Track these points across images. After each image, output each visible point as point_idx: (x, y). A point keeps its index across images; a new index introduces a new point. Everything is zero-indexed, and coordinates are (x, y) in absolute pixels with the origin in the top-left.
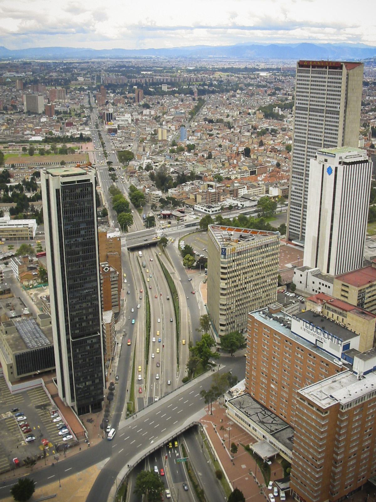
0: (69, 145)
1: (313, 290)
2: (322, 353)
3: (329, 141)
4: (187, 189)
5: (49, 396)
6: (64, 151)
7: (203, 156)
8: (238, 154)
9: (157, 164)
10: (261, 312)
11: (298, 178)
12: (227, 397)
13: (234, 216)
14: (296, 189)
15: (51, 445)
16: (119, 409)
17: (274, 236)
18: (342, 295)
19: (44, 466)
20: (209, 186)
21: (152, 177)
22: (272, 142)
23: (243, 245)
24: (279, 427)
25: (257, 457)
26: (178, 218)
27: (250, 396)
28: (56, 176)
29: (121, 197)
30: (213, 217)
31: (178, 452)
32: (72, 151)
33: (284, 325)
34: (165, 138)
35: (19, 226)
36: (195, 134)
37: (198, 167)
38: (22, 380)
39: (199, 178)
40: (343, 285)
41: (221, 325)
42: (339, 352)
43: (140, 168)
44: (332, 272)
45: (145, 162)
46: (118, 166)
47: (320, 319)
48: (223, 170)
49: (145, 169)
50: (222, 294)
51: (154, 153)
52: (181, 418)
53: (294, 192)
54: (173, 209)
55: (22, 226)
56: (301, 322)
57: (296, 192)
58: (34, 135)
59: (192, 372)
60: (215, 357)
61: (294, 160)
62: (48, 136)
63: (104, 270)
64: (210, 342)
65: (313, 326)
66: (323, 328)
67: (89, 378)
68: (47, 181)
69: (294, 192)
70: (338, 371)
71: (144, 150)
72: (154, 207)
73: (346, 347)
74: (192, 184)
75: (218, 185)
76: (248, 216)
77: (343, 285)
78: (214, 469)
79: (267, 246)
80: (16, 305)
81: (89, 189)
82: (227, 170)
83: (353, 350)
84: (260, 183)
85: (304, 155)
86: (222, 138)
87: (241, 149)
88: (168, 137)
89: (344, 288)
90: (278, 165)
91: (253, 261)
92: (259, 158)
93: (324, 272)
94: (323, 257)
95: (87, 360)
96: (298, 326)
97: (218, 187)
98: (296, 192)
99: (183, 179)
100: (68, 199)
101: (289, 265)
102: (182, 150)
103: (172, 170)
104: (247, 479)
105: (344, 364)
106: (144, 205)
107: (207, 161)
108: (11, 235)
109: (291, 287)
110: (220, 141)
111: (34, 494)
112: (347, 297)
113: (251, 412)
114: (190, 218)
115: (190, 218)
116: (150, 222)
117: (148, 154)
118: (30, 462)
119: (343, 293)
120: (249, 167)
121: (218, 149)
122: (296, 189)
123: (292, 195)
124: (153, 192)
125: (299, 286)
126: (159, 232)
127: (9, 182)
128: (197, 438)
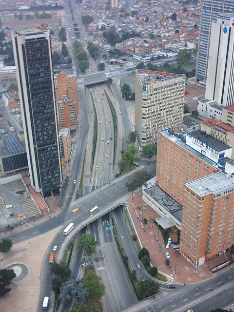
0: (48, 12)
1: (211, 116)
2: (205, 160)
3: (228, 8)
4: (129, 43)
5: (25, 185)
6: (44, 17)
7: (143, 19)
8: (167, 18)
9: (109, 25)
10: (167, 131)
11: (205, 36)
12: (144, 188)
13: (160, 63)
14: (203, 44)
15: (25, 217)
16: (72, 194)
17: (181, 78)
18: (228, 120)
19: (20, 231)
20: (145, 41)
21: (105, 35)
22: (193, 9)
23: (159, 84)
24: (177, 208)
25: (160, 228)
26: (121, 65)
27: (159, 187)
28: (21, 35)
29: (82, 49)
30: (145, 64)
31: (109, 222)
32: (49, 16)
33: (182, 140)
34: (116, 6)
35: (10, 71)
36: (138, 3)
37: (138, 27)
38: (8, 175)
39: (138, 35)
40: (229, 113)
41: (143, 139)
42: (216, 158)
43: (97, 28)
44: (225, 104)
45: (100, 24)
46: (81, 27)
47: (205, 136)
48: (156, 29)
49: (100, 29)
50: (143, 118)
51: (108, 18)
52: (111, 200)
53: (201, 46)
54: (117, 58)
55: (12, 71)
56: (193, 138)
57: (203, 46)
58: (23, 5)
59: (122, 171)
60: (138, 160)
61: (202, 22)
62: (33, 5)
63: (64, 100)
64: (134, 151)
65: (200, 141)
66: (207, 142)
67: (50, 173)
68: (16, 38)
69: (201, 46)
70: (215, 172)
71: (101, 15)
72: (105, 56)
73: (222, 156)
74: (133, 40)
75: (151, 41)
76: (170, 63)
77: (229, 113)
78: (132, 234)
79: (175, 84)
80: (5, 125)
81: (45, 44)
82: (159, 30)
83: (227, 158)
84: (181, 39)
85: (209, 18)
86: (157, 6)
87: (170, 14)
88: (118, 5)
89: (229, 119)
90: (196, 26)
91: (165, 95)
92: (183, 21)
93: (219, 103)
94: (218, 92)
95: (49, 161)
96: (190, 141)
97: (151, 42)
98: (203, 46)
99: (126, 36)
100: (30, 52)
101: (196, 99)
102: (128, 15)
103: (119, 29)
104: (152, 241)
105: (219, 167)
106: (97, 55)
107: (145, 23)
108: (4, 77)
109: (195, 114)
110: (156, 9)
111: (12, 248)
112: (231, 121)
113: (158, 198)
114: (130, 64)
115: (130, 64)
116: (101, 67)
117: (103, 18)
118: (10, 228)
119: (229, 119)
120: (174, 28)
121: (154, 14)
122: (203, 44)
123: (200, 48)
124: (105, 46)
125: (201, 113)
126: (108, 74)
127: (4, 40)
128: (123, 214)
